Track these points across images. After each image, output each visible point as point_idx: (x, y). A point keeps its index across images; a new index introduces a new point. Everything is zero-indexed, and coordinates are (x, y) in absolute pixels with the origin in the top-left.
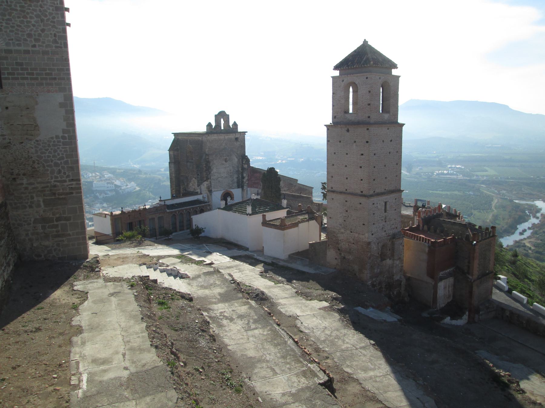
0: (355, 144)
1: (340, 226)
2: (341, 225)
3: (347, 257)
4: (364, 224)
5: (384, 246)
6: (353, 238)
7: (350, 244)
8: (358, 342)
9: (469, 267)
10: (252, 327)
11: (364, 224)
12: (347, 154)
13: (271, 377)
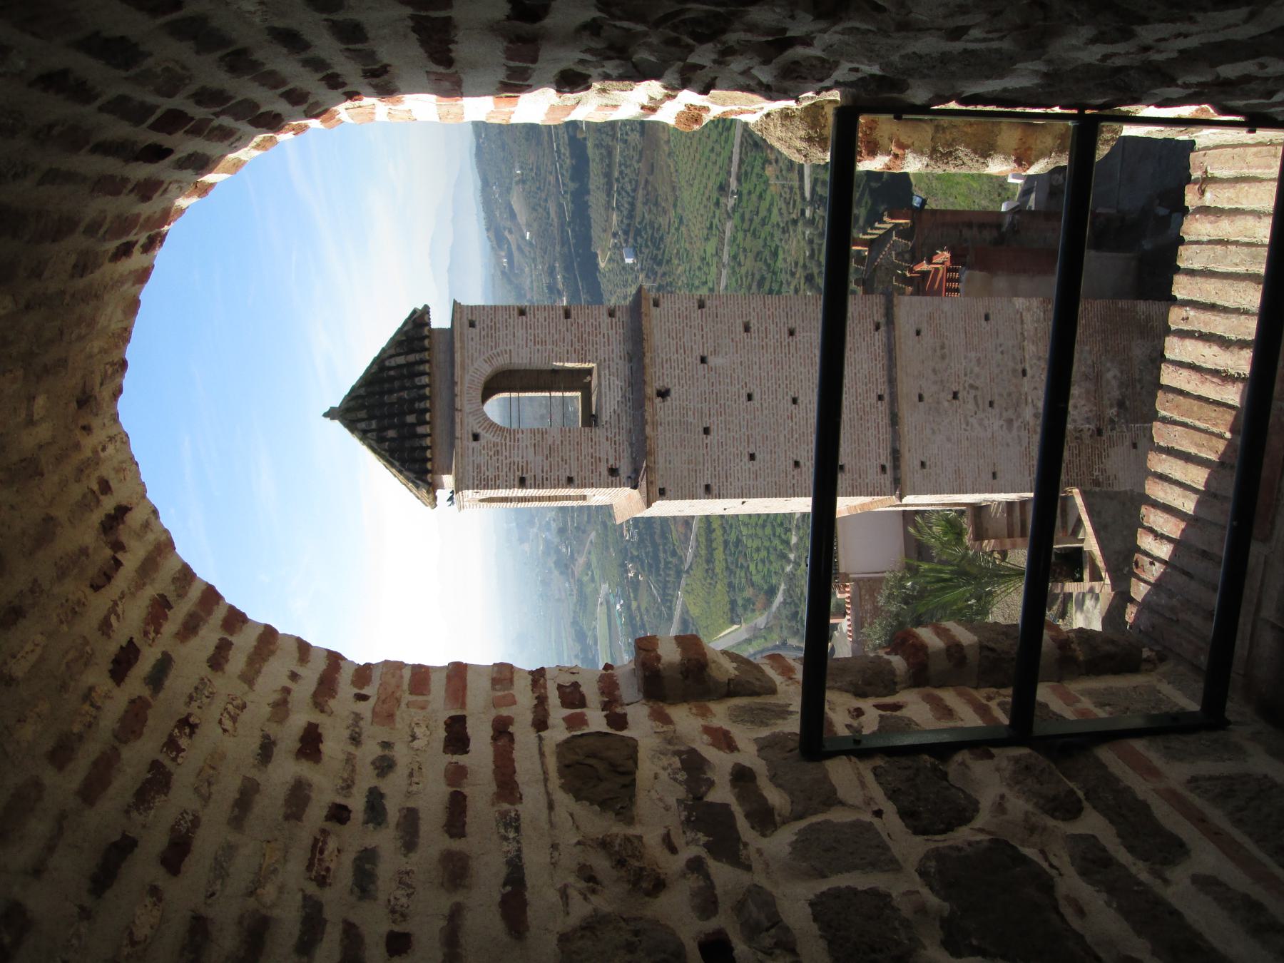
0: (712, 360)
1: (1016, 424)
12: (750, 397)
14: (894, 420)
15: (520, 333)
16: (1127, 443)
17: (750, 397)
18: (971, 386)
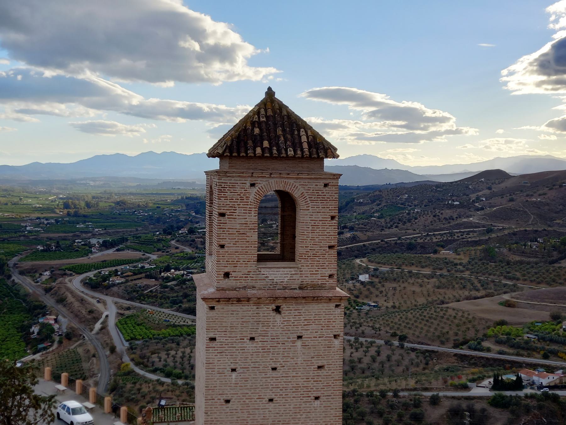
0: (299, 343)
12: (274, 369)
17: (274, 369)
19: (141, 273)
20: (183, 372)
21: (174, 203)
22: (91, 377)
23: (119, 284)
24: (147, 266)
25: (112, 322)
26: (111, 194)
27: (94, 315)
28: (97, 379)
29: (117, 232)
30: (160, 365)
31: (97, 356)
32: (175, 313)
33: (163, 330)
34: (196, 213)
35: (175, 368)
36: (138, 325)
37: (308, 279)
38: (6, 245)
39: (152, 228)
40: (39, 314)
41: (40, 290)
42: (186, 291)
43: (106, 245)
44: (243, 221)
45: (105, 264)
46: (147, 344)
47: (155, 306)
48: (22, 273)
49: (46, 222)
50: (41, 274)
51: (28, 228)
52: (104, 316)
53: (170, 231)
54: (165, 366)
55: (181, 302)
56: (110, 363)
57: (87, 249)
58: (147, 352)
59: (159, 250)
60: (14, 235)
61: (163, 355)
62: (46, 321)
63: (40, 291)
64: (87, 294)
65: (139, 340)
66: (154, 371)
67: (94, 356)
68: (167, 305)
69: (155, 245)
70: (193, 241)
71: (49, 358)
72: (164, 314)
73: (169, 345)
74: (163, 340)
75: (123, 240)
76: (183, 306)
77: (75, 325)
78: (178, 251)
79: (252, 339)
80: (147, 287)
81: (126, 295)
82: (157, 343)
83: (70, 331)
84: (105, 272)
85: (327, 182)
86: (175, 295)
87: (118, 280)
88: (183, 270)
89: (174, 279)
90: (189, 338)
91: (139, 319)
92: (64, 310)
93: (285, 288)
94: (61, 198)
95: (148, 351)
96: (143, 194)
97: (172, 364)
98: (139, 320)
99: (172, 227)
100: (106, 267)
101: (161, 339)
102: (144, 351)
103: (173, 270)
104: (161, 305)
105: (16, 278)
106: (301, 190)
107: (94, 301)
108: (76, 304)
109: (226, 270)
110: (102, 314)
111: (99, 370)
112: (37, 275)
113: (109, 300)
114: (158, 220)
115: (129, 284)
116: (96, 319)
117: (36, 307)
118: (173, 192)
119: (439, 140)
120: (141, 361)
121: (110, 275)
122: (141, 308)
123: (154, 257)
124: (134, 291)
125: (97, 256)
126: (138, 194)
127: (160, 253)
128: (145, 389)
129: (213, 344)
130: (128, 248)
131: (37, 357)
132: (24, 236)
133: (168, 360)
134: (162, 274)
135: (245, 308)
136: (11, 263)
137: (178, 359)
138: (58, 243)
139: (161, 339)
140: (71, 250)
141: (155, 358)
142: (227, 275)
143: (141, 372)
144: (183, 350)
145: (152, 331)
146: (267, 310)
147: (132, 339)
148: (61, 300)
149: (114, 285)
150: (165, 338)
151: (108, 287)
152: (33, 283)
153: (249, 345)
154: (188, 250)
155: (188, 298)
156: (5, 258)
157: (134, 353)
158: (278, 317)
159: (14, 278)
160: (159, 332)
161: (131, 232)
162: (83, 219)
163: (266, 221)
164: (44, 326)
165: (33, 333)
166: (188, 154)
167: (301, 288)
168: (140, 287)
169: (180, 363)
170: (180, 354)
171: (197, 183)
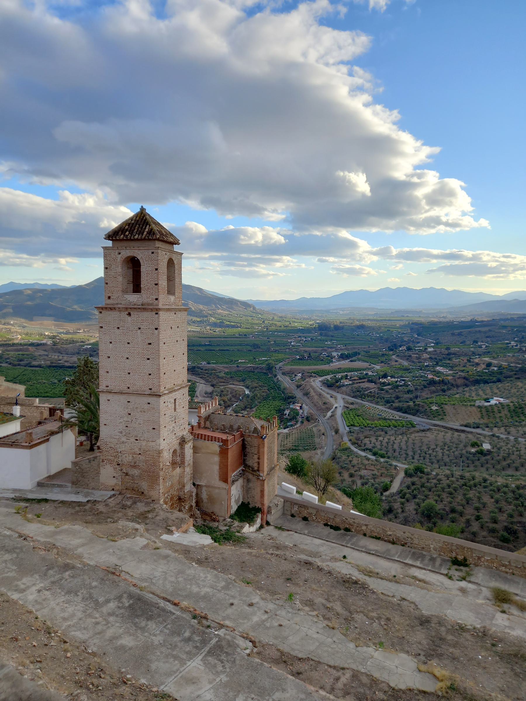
0: (139, 331)
1: (121, 435)
2: (121, 433)
3: (130, 473)
4: (154, 429)
5: (175, 452)
6: (139, 447)
7: (135, 456)
8: (215, 582)
9: (259, 463)
10: (100, 600)
11: (154, 429)
12: (129, 343)
13: (182, 669)
14: (121, 393)
15: (150, 269)
16: (115, 475)
17: (129, 343)
18: (132, 420)
19: (365, 378)
20: (387, 454)
21: (401, 327)
22: (320, 448)
23: (347, 385)
24: (370, 373)
25: (339, 412)
26: (353, 320)
27: (326, 407)
28: (324, 450)
29: (354, 348)
30: (370, 446)
31: (325, 434)
32: (387, 410)
33: (376, 422)
34: (418, 335)
35: (381, 450)
36: (358, 416)
37: (146, 301)
38: (276, 355)
39: (381, 346)
40: (291, 402)
41: (294, 386)
42: (398, 394)
43: (343, 357)
44: (115, 271)
45: (340, 370)
46: (362, 430)
47: (372, 403)
48: (283, 374)
49: (304, 340)
50: (296, 375)
51: (292, 343)
52: (334, 407)
53: (393, 348)
54: (374, 447)
55: (393, 402)
56: (334, 440)
57: (330, 359)
58: (361, 436)
59: (382, 362)
60: (283, 348)
61: (373, 440)
62: (294, 407)
63: (293, 387)
64: (324, 391)
65: (357, 426)
66: (364, 450)
67: (323, 434)
68: (381, 403)
69: (380, 358)
70: (410, 356)
71: (293, 432)
72: (378, 410)
73: (378, 433)
74: (375, 429)
75: (356, 354)
76: (394, 405)
77: (314, 411)
78: (397, 363)
79: (118, 328)
80: (368, 388)
81: (352, 394)
82: (370, 430)
83: (309, 415)
84: (339, 376)
85: (153, 251)
86: (389, 396)
87: (347, 382)
88: (398, 378)
89: (389, 384)
90: (396, 429)
91: (359, 412)
92: (308, 400)
93: (135, 305)
94: (318, 323)
95: (363, 435)
96: (378, 320)
97: (379, 447)
98: (359, 413)
99: (395, 345)
100: (340, 373)
101: (373, 428)
102: (359, 435)
103: (389, 378)
104: (377, 403)
105: (280, 377)
106: (141, 255)
107: (329, 396)
108: (316, 397)
109: (109, 295)
110: (333, 405)
111: (325, 444)
112: (293, 376)
113: (339, 396)
114: (387, 340)
115: (354, 385)
116: (328, 409)
117: (289, 398)
118: (403, 318)
119: (318, 233)
120: (356, 441)
121: (342, 378)
122: (362, 404)
123: (377, 367)
124: (358, 391)
125: (336, 364)
126: (374, 320)
127: (383, 364)
128: (355, 462)
129: (101, 330)
130: (359, 360)
131: (286, 431)
132: (289, 349)
133: (377, 443)
134: (381, 380)
135: (115, 313)
136: (278, 367)
137: (384, 444)
138: (310, 354)
139: (373, 428)
140: (319, 360)
141: (367, 441)
142: (109, 298)
143: (355, 450)
144: (388, 437)
145: (368, 421)
146: (124, 314)
147: (352, 425)
148: (306, 394)
149: (343, 386)
150: (376, 427)
151: (339, 387)
152: (290, 381)
153: (117, 331)
154: (406, 363)
155: (399, 399)
156: (274, 363)
157: (352, 436)
158: (129, 318)
159: (278, 377)
160: (373, 422)
161: (364, 348)
162: (331, 338)
163: (477, 342)
164: (293, 410)
165: (286, 415)
166: (418, 289)
167: (142, 305)
168: (362, 388)
169: (385, 447)
170: (386, 440)
171: (424, 311)
